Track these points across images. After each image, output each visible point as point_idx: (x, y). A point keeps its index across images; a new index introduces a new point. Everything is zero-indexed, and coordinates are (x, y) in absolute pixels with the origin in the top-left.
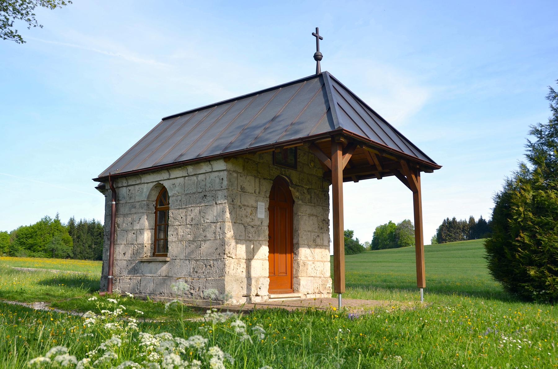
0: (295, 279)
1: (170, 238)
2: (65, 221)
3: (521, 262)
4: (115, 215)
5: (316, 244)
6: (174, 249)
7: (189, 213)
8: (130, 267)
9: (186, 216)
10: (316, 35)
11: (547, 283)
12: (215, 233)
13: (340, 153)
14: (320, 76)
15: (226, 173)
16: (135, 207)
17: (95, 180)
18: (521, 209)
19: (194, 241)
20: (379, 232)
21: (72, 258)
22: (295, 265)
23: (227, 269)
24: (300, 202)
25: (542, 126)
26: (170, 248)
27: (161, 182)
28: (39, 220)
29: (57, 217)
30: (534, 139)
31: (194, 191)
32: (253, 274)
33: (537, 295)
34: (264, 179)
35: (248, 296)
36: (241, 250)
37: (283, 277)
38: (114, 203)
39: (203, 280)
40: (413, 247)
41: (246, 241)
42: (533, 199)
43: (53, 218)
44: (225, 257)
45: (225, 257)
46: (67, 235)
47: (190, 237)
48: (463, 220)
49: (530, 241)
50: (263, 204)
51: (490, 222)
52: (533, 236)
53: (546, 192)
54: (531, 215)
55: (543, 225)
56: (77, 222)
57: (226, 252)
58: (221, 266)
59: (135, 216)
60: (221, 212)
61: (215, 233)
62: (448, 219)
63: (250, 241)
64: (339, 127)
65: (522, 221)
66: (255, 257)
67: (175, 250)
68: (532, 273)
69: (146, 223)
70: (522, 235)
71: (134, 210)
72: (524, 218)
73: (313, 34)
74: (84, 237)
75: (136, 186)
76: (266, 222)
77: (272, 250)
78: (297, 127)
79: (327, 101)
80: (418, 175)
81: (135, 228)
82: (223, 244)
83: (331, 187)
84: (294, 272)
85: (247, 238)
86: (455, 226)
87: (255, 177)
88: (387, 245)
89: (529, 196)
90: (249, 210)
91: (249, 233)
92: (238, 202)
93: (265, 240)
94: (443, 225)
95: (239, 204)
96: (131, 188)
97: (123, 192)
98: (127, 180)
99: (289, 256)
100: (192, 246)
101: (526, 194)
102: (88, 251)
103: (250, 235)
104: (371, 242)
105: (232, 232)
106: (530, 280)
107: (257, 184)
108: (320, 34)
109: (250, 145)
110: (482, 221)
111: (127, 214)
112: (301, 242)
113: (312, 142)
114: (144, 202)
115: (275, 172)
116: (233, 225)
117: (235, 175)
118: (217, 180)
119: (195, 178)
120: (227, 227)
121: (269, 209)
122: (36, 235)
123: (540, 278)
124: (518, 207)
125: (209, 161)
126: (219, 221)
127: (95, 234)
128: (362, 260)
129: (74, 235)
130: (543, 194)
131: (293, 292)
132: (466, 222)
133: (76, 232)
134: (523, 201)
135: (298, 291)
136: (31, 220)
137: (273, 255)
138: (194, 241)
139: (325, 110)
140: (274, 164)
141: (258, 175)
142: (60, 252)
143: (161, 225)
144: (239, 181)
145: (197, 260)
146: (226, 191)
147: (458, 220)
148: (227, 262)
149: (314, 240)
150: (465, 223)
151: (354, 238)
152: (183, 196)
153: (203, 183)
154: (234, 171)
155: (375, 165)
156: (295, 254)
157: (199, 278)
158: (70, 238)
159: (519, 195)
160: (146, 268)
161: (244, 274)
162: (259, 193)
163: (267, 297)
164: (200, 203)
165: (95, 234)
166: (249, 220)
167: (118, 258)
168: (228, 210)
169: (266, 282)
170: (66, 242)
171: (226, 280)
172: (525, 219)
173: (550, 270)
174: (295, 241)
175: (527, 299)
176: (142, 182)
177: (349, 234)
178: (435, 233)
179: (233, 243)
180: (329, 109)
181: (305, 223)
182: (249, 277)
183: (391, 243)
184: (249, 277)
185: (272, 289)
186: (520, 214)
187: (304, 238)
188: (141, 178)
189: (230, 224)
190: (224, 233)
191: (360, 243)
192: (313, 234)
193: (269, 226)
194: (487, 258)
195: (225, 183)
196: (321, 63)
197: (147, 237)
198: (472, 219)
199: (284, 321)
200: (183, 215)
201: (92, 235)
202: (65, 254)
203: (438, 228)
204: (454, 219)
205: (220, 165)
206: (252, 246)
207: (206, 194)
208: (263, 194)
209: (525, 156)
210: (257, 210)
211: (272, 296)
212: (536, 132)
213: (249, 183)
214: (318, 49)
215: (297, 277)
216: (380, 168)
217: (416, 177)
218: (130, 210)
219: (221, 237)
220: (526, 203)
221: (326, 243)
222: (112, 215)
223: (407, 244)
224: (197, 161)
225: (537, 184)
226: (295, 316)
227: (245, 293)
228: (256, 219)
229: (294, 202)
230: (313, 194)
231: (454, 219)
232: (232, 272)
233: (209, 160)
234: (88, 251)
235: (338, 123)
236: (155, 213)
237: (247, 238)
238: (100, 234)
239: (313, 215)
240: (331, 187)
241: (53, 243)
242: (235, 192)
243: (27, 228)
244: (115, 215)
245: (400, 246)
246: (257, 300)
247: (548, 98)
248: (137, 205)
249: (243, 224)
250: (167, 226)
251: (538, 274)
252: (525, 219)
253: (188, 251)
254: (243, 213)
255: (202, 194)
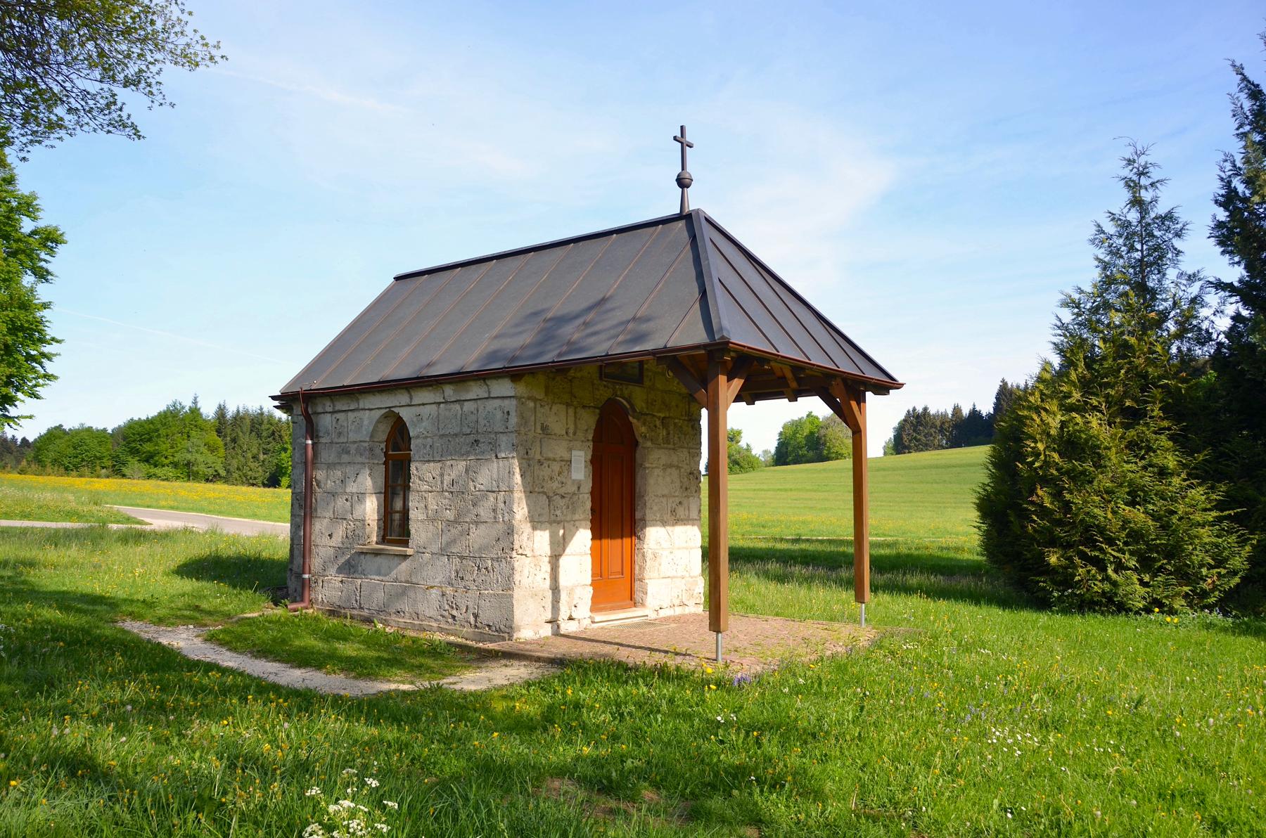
0: (637, 584)
1: (413, 514)
2: (208, 410)
3: (1035, 539)
4: (313, 463)
5: (675, 518)
6: (420, 530)
7: (448, 470)
8: (342, 560)
9: (442, 475)
10: (682, 141)
11: (1077, 578)
12: (494, 511)
13: (722, 379)
14: (686, 218)
15: (514, 402)
16: (348, 453)
17: (274, 398)
18: (1041, 446)
19: (456, 522)
20: (790, 432)
21: (226, 480)
22: (638, 559)
23: (517, 577)
24: (649, 444)
25: (1082, 292)
26: (413, 531)
27: (396, 410)
28: (163, 408)
29: (195, 402)
30: (1067, 316)
31: (457, 430)
32: (563, 581)
33: (1059, 597)
34: (584, 407)
35: (553, 621)
36: (541, 540)
37: (618, 584)
38: (310, 442)
39: (473, 594)
40: (848, 463)
41: (551, 523)
42: (1062, 428)
43: (188, 404)
44: (514, 554)
45: (514, 554)
46: (213, 437)
47: (450, 515)
48: (942, 410)
49: (1052, 503)
50: (582, 453)
51: (989, 415)
52: (1057, 495)
53: (1083, 416)
54: (1056, 456)
55: (1075, 476)
56: (231, 411)
57: (516, 546)
58: (507, 571)
59: (348, 469)
60: (506, 473)
61: (494, 511)
62: (914, 409)
63: (559, 523)
64: (723, 337)
65: (1041, 467)
66: (568, 551)
67: (423, 535)
68: (1053, 560)
69: (369, 483)
70: (1040, 492)
71: (345, 458)
72: (1045, 461)
73: (675, 138)
74: (244, 439)
75: (350, 414)
76: (587, 486)
77: (598, 534)
78: (644, 327)
79: (700, 276)
80: (861, 400)
81: (348, 490)
82: (510, 531)
83: (704, 412)
84: (637, 572)
85: (553, 518)
86: (927, 423)
87: (568, 405)
88: (804, 456)
89: (1054, 422)
90: (556, 467)
91: (556, 508)
92: (535, 453)
93: (584, 519)
94: (905, 420)
95: (538, 457)
96: (341, 416)
97: (325, 422)
98: (332, 401)
99: (627, 541)
100: (453, 531)
101: (1050, 420)
102: (252, 465)
103: (558, 513)
104: (773, 451)
105: (526, 510)
106: (1049, 571)
107: (571, 419)
108: (689, 138)
109: (560, 355)
110: (975, 414)
111: (334, 464)
112: (649, 516)
113: (671, 359)
114: (366, 445)
115: (604, 393)
116: (527, 498)
117: (531, 404)
118: (499, 415)
119: (457, 406)
120: (516, 500)
121: (592, 462)
122: (159, 436)
123: (1066, 568)
124: (1036, 442)
125: (484, 380)
126: (501, 489)
127: (265, 434)
128: (757, 487)
129: (225, 436)
130: (1079, 419)
131: (635, 605)
132: (946, 414)
133: (229, 431)
134: (1044, 431)
135: (643, 605)
136: (147, 408)
137: (598, 542)
138: (456, 522)
139: (697, 295)
140: (601, 378)
141: (572, 402)
142: (202, 469)
143: (396, 483)
144: (539, 415)
145: (462, 558)
146: (514, 435)
147: (932, 411)
148: (516, 564)
149: (673, 511)
150: (945, 415)
151: (743, 444)
152: (436, 438)
153: (473, 418)
154: (529, 398)
155: (784, 377)
156: (639, 538)
157: (467, 589)
158: (220, 442)
159: (1038, 421)
160: (367, 562)
161: (548, 582)
162: (575, 434)
163: (589, 621)
164: (468, 453)
165: (265, 434)
166: (555, 485)
167: (318, 541)
168: (517, 470)
169: (586, 595)
170: (212, 449)
171: (515, 596)
172: (1047, 464)
173: (1083, 556)
174: (638, 515)
175: (1041, 603)
176: (361, 406)
177: (734, 437)
178: (891, 435)
179: (526, 528)
180: (703, 293)
181: (657, 481)
182: (555, 589)
183: (811, 454)
184: (555, 589)
185: (596, 605)
186: (1037, 455)
187: (655, 508)
188: (358, 400)
189: (523, 495)
190: (511, 511)
191: (753, 453)
192: (671, 500)
193: (592, 493)
194: (979, 528)
195: (514, 420)
196: (690, 191)
197: (371, 508)
198: (957, 410)
199: (621, 692)
200: (436, 473)
201: (259, 436)
202: (211, 471)
203: (896, 425)
204: (925, 409)
205: (503, 387)
206: (561, 532)
207: (479, 437)
208: (580, 434)
209: (1052, 346)
210: (570, 466)
211: (598, 618)
212: (1070, 303)
213: (558, 419)
214: (683, 168)
215: (641, 580)
216: (794, 385)
217: (859, 404)
218: (339, 456)
219: (506, 518)
220: (1048, 435)
221: (694, 515)
222: (306, 463)
223: (839, 456)
224: (459, 378)
225: (1069, 401)
226: (640, 681)
227: (549, 616)
228: (569, 482)
229: (637, 443)
230: (672, 427)
231: (925, 409)
232: (525, 582)
233: (481, 376)
234: (252, 465)
235: (721, 329)
236: (385, 463)
237: (553, 518)
238: (273, 433)
239: (671, 466)
240: (704, 412)
241: (189, 452)
242: (531, 434)
243: (140, 423)
244: (313, 463)
245: (827, 459)
246: (567, 627)
247: (1093, 241)
248: (353, 448)
249: (544, 493)
250: (406, 488)
251: (1064, 562)
252: (1047, 464)
253: (445, 539)
254: (545, 472)
255: (472, 438)
